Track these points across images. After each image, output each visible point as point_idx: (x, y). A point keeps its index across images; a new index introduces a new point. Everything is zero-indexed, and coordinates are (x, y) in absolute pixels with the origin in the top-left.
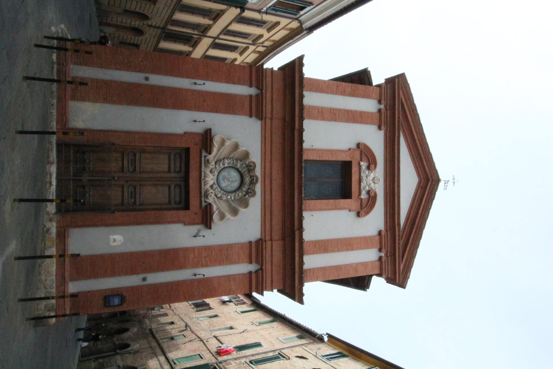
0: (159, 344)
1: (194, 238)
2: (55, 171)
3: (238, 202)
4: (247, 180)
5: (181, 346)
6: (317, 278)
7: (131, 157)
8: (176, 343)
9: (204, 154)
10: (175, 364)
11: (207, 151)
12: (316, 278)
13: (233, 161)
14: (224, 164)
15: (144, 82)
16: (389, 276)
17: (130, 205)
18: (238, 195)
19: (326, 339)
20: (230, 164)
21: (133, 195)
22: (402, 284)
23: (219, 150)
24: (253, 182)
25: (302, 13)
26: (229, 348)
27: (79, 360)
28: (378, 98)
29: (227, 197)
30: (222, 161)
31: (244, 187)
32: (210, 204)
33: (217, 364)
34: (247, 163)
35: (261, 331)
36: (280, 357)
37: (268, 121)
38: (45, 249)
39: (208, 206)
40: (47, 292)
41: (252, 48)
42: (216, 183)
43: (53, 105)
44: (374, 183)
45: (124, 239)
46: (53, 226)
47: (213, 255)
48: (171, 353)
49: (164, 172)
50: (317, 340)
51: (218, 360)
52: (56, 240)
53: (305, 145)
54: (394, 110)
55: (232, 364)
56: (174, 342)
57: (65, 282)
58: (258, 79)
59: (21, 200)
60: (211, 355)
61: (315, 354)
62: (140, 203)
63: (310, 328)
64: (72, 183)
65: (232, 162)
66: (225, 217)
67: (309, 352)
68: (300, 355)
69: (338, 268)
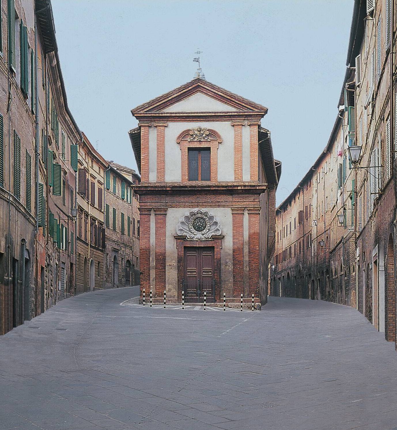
4: (199, 215)
64: (201, 297)
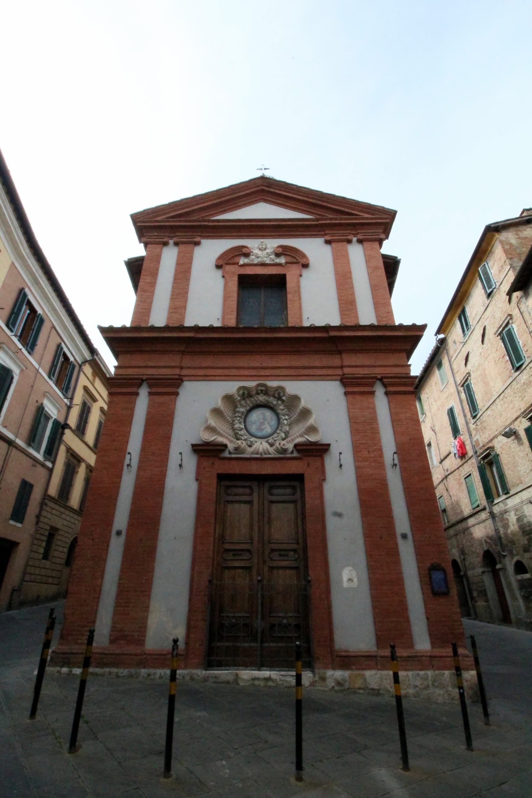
0: (453, 525)
1: (342, 467)
2: (248, 672)
3: (292, 412)
4: (262, 398)
5: (455, 500)
6: (388, 312)
7: (229, 556)
8: (450, 507)
9: (226, 454)
10: (478, 506)
11: (223, 451)
12: (389, 314)
14: (241, 429)
15: (123, 537)
16: (381, 231)
17: (299, 557)
18: (283, 410)
19: (442, 336)
20: (241, 420)
21: (283, 553)
22: (390, 215)
23: (221, 435)
24: (266, 391)
25: (72, 359)
26: (457, 444)
27: (475, 619)
28: (161, 246)
29: (285, 425)
30: (237, 431)
31: (272, 403)
32: (296, 446)
33: (478, 456)
34: (239, 398)
35: (433, 410)
36: (466, 383)
37: (184, 372)
38: (367, 687)
39: (298, 448)
40: (433, 685)
42: (265, 440)
43: (149, 675)
44: (265, 249)
45: (349, 565)
46: (333, 675)
47: (365, 442)
48: (464, 512)
49: (251, 509)
50: (443, 346)
51: (472, 456)
52: (352, 670)
53: (217, 324)
54: (176, 227)
55: (477, 439)
56: (448, 509)
57: (417, 656)
58: (128, 385)
59: (299, 766)
60: (465, 465)
61: (461, 345)
62: (295, 543)
63: (428, 356)
64: (267, 644)
65: (238, 419)
66: (313, 425)
67: (459, 353)
68: (464, 362)
69: (374, 288)
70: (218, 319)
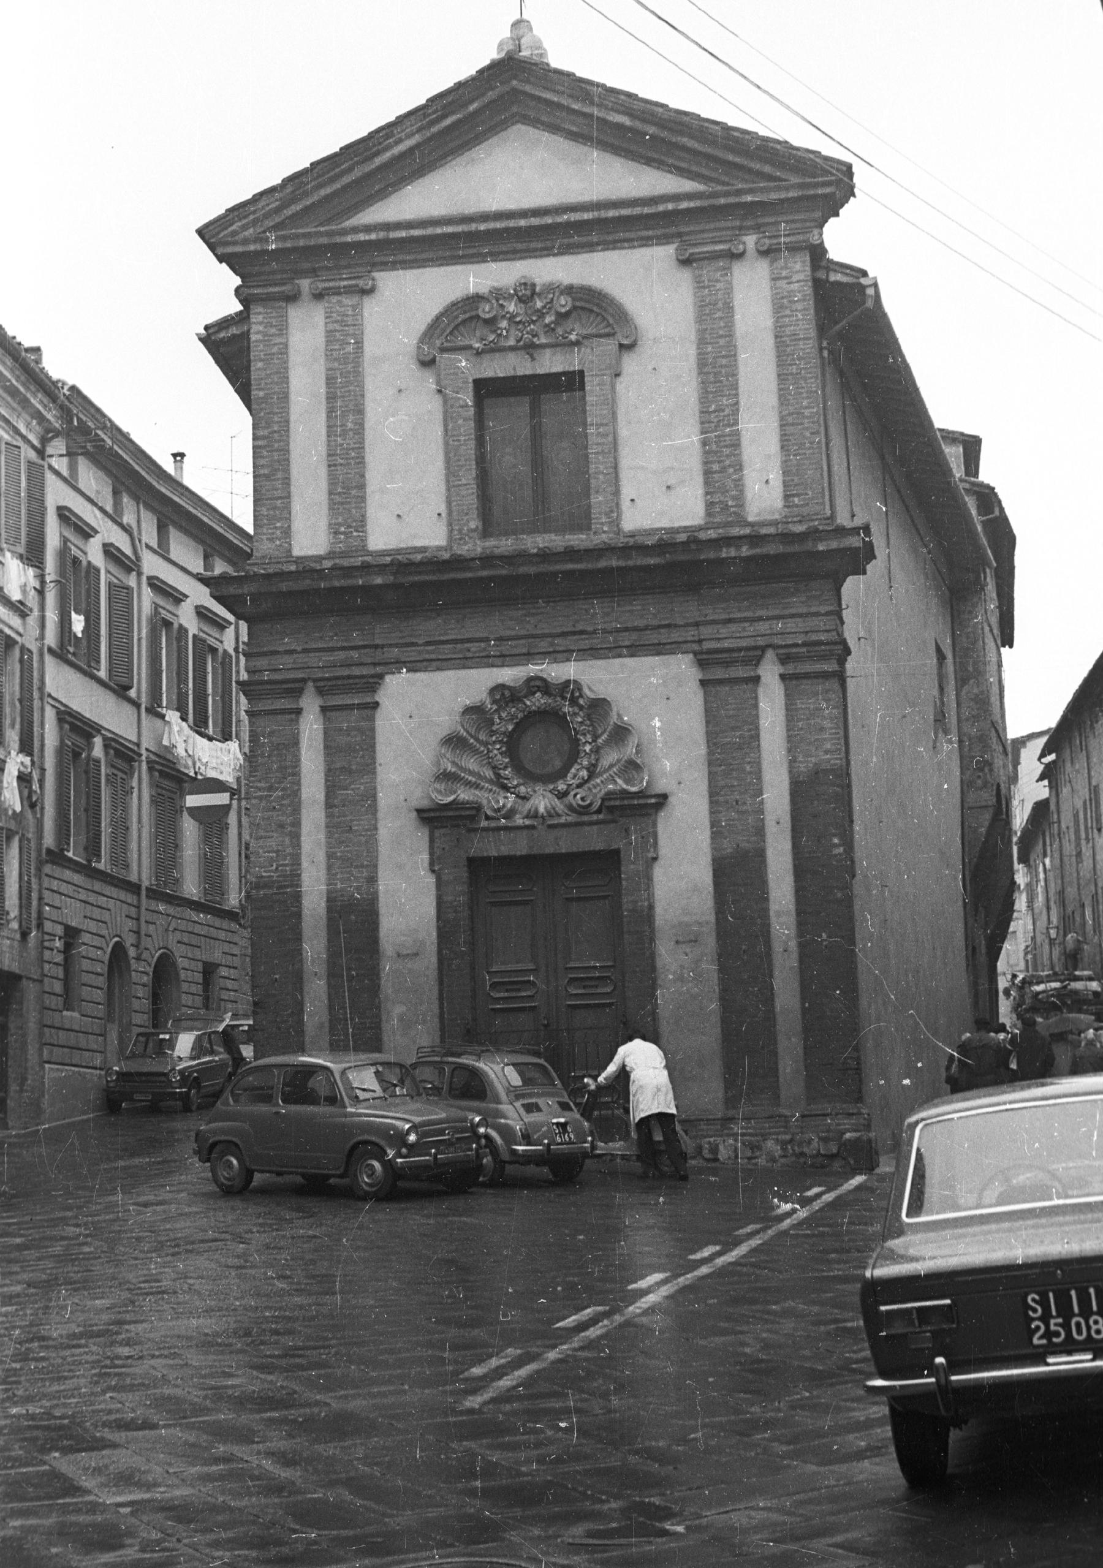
13: (494, 742)
41: (152, 565)
65: (498, 746)
70: (439, 515)
